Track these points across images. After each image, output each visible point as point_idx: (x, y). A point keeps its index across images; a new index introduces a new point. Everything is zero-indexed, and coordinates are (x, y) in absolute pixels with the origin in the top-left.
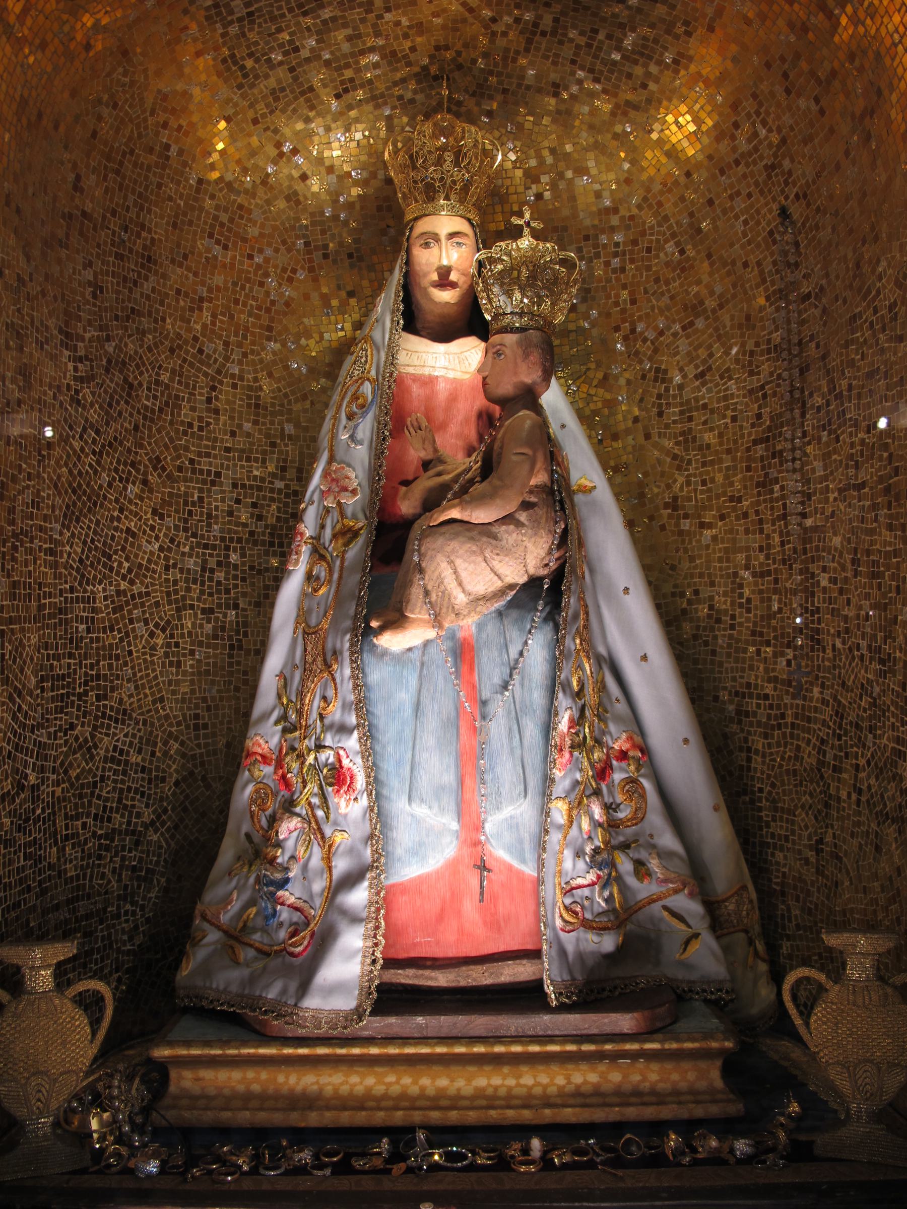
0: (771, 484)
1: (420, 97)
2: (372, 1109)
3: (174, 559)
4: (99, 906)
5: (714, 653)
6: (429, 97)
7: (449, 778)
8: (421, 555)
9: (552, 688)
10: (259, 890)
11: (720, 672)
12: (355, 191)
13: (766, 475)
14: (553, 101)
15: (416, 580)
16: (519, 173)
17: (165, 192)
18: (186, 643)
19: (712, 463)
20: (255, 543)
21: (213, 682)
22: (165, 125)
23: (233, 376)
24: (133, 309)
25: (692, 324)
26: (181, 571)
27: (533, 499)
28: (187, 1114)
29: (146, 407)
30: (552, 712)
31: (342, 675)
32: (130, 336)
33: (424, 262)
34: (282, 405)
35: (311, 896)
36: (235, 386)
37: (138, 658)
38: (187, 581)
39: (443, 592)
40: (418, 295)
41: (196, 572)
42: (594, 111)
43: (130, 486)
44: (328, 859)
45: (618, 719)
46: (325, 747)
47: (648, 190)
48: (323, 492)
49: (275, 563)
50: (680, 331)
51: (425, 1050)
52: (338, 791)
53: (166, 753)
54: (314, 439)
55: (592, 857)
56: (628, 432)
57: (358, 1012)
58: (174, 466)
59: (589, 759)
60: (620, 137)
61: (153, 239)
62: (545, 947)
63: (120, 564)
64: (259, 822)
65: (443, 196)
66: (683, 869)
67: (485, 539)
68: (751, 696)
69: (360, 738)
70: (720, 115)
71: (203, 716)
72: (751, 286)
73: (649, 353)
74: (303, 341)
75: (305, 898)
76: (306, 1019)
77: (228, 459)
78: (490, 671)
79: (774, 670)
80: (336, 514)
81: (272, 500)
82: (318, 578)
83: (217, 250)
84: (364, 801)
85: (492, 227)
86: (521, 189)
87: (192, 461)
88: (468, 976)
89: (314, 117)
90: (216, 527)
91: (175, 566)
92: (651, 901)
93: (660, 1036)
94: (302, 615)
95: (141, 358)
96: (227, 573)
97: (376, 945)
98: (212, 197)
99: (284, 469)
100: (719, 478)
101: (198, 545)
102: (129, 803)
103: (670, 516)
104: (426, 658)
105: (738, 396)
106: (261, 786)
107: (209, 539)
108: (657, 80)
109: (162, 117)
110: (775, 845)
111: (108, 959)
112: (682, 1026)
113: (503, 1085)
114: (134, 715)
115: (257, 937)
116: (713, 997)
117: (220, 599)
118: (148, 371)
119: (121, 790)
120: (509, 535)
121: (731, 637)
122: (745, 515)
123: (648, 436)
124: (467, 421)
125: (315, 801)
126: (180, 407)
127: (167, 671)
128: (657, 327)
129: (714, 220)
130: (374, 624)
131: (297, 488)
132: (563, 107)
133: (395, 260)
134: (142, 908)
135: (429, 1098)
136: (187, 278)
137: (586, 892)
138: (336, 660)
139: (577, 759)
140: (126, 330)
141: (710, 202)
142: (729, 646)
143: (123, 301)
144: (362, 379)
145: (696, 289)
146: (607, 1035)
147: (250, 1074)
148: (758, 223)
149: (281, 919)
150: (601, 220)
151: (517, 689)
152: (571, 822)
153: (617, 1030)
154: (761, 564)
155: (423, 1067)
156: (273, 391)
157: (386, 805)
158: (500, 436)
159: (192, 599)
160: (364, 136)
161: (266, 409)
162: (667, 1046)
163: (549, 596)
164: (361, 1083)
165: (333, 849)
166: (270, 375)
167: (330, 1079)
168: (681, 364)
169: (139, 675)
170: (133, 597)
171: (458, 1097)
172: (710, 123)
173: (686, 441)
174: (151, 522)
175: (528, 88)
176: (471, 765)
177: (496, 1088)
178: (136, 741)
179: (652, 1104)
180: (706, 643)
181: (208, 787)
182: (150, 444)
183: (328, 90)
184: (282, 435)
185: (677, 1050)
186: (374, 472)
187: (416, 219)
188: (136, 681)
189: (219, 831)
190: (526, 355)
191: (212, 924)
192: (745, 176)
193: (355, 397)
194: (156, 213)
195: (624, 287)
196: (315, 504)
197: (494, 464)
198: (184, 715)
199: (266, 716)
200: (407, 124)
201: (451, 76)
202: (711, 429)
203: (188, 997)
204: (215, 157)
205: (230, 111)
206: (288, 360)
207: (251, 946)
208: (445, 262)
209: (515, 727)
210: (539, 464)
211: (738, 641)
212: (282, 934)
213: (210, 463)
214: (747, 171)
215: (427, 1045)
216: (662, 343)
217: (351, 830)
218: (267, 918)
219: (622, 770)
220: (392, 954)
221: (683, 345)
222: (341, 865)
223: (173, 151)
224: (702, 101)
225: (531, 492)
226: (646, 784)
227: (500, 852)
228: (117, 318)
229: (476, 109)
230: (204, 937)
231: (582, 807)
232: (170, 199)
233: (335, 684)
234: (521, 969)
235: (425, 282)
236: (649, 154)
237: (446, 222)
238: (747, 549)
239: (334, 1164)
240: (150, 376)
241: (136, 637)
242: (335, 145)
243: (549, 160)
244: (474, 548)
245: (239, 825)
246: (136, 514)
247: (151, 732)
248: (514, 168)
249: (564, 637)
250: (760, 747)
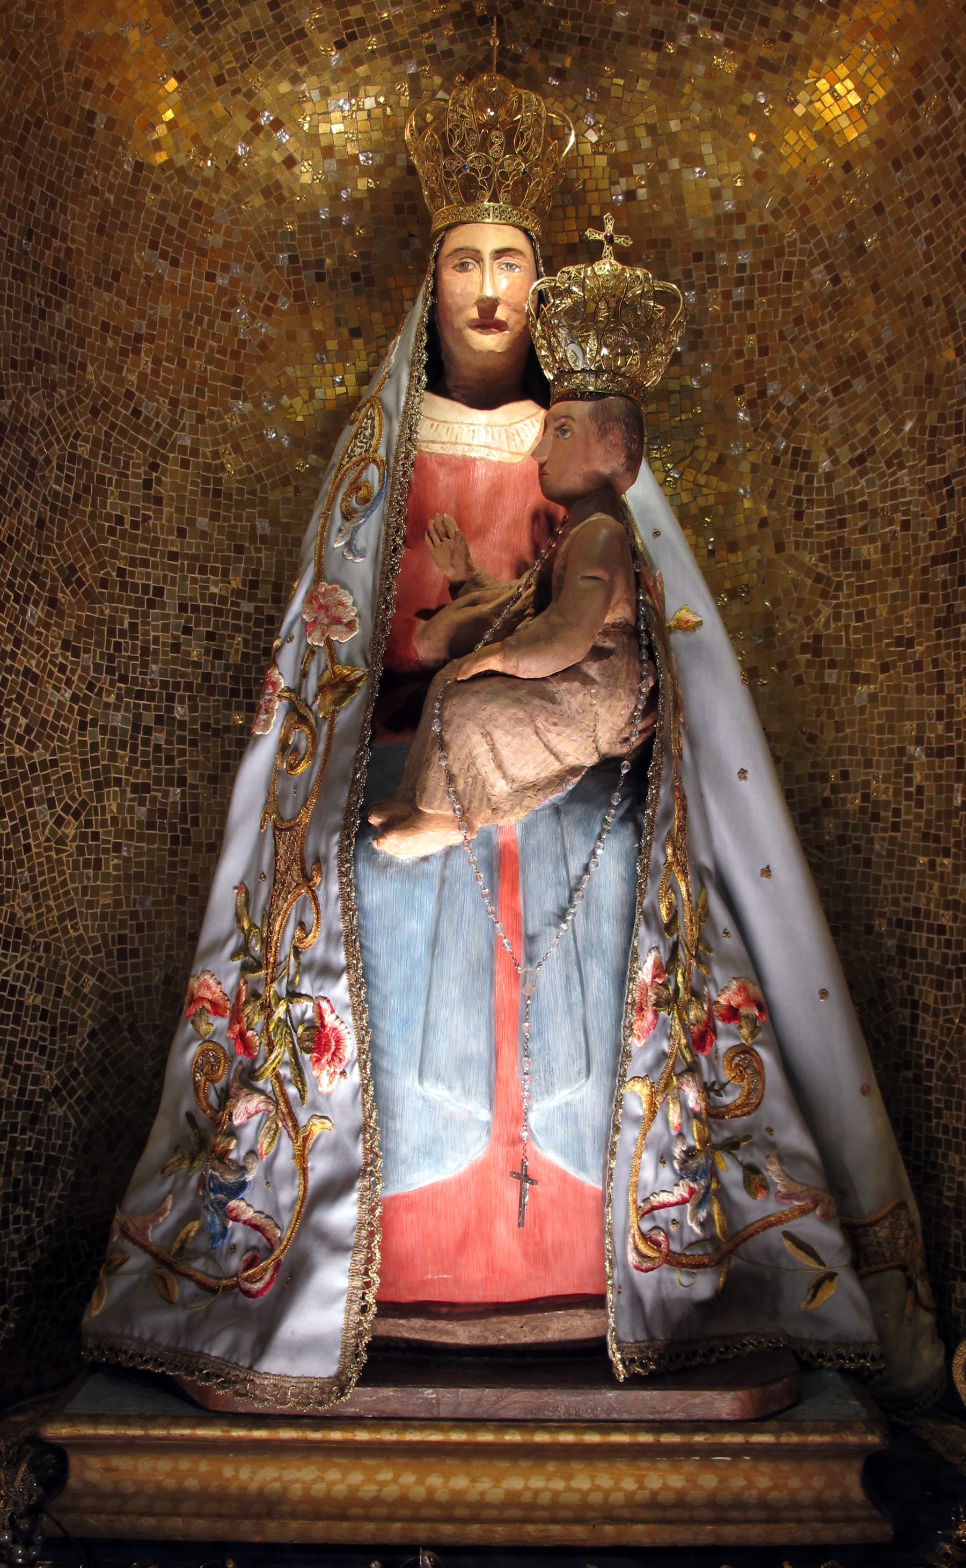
0: (957, 623)
1: (459, 48)
3: (93, 713)
5: (867, 863)
6: (472, 48)
7: (478, 1046)
8: (444, 724)
9: (633, 915)
10: (203, 1198)
11: (877, 892)
12: (364, 184)
13: (950, 608)
14: (652, 57)
15: (435, 759)
16: (602, 161)
17: (87, 181)
18: (108, 833)
19: (872, 588)
20: (211, 691)
21: (147, 891)
22: (88, 84)
23: (183, 449)
24: (38, 351)
25: (847, 385)
26: (104, 730)
27: (609, 644)
28: (92, 1520)
29: (56, 494)
30: (629, 955)
31: (327, 893)
32: (33, 391)
33: (458, 291)
34: (253, 493)
35: (277, 1210)
36: (185, 464)
37: (39, 855)
38: (111, 744)
39: (475, 778)
40: (449, 339)
41: (124, 731)
42: (712, 73)
43: (30, 608)
44: (301, 1157)
45: (727, 961)
46: (300, 995)
47: (789, 189)
48: (305, 624)
49: (239, 720)
50: (830, 395)
51: (435, 1437)
52: (318, 1060)
53: (77, 992)
54: (298, 542)
55: (683, 1162)
56: (751, 539)
57: (339, 1383)
58: (94, 578)
59: (682, 1020)
60: (751, 112)
61: (69, 250)
62: (610, 1296)
63: (15, 720)
64: (206, 1098)
65: (488, 195)
66: (816, 1181)
67: (537, 702)
68: (919, 927)
69: (351, 985)
70: (896, 81)
71: (132, 939)
72: (934, 333)
73: (785, 426)
74: (285, 400)
75: (268, 1212)
76: (264, 1390)
77: (173, 569)
78: (541, 892)
79: (954, 891)
80: (324, 657)
81: (237, 629)
82: (296, 749)
83: (163, 266)
84: (355, 1077)
85: (562, 239)
86: (604, 184)
87: (121, 572)
88: (500, 1331)
89: (306, 75)
90: (154, 667)
91: (94, 723)
92: (767, 1224)
93: (774, 1424)
94: (273, 801)
95: (49, 422)
96: (170, 734)
97: (367, 1285)
98: (156, 189)
99: (254, 585)
100: (882, 610)
101: (129, 692)
102: (23, 1063)
103: (810, 664)
104: (448, 872)
105: (912, 493)
106: (210, 1046)
107: (144, 684)
108: (805, 29)
109: (83, 72)
110: (948, 1143)
112: (805, 1411)
113: (546, 1489)
114: (32, 937)
115: (199, 1264)
116: (853, 1366)
117: (159, 770)
118: (58, 441)
119: (12, 1044)
120: (573, 697)
121: (893, 841)
122: (919, 666)
123: (780, 547)
124: (516, 524)
125: (286, 1072)
126: (105, 494)
127: (81, 874)
128: (797, 388)
129: (883, 237)
130: (375, 820)
131: (273, 613)
132: (667, 66)
133: (419, 285)
134: (40, 1212)
135: (439, 1505)
136: (118, 307)
137: (673, 1213)
138: (319, 870)
139: (665, 1021)
140: (28, 383)
141: (879, 209)
142: (890, 854)
143: (24, 340)
144: (366, 461)
145: (854, 335)
146: (698, 1421)
147: (184, 1464)
148: (948, 241)
149: (234, 1241)
150: (719, 232)
151: (580, 921)
152: (654, 1113)
153: (712, 1415)
154: (939, 738)
155: (432, 1460)
156: (240, 472)
157: (385, 1081)
158: (562, 550)
159: (118, 770)
160: (378, 103)
161: (229, 497)
162: (784, 1439)
163: (627, 786)
164: (342, 1481)
165: (310, 1143)
166: (237, 449)
167: (298, 1475)
168: (831, 443)
169: (40, 879)
170: (33, 767)
171: (482, 1504)
172: (881, 92)
173: (835, 555)
174: (61, 659)
175: (617, 36)
176: (511, 1028)
177: (537, 1493)
178: (34, 974)
179: (760, 1521)
180: (857, 849)
181: (137, 1040)
182: (60, 547)
183: (325, 36)
184: (253, 537)
185: (798, 1445)
186: (380, 596)
187: (449, 228)
188: (36, 888)
189: (150, 1104)
190: (603, 433)
192: (929, 172)
193: (356, 487)
194: (73, 212)
195: (751, 329)
196: (295, 641)
197: (554, 591)
198: (104, 937)
199: (218, 946)
200: (441, 87)
201: (504, 18)
202: (872, 540)
203: (98, 1348)
204: (161, 130)
205: (183, 66)
206: (263, 427)
207: (190, 1277)
208: (489, 292)
209: (575, 976)
210: (619, 594)
211: (903, 847)
212: (235, 1263)
213: (148, 574)
214: (934, 165)
215: (439, 1429)
216: (803, 412)
217: (336, 1117)
218: (213, 1238)
219: (730, 1034)
220: (391, 1296)
221: (834, 416)
222: (321, 1167)
223: (100, 123)
224: (870, 60)
225: (606, 633)
226: (765, 1055)
227: (549, 1153)
228: (14, 364)
229: (540, 67)
230: (124, 1261)
231: (669, 1091)
232: (95, 191)
233: (317, 906)
234: (577, 1322)
235: (459, 321)
236: (791, 137)
237: (491, 234)
238: (920, 715)
240: (63, 449)
241: (35, 826)
242: (336, 116)
243: (646, 143)
244: (521, 714)
245: (177, 1102)
246: (39, 648)
247: (56, 962)
248: (595, 153)
249: (649, 845)
250: (931, 1002)
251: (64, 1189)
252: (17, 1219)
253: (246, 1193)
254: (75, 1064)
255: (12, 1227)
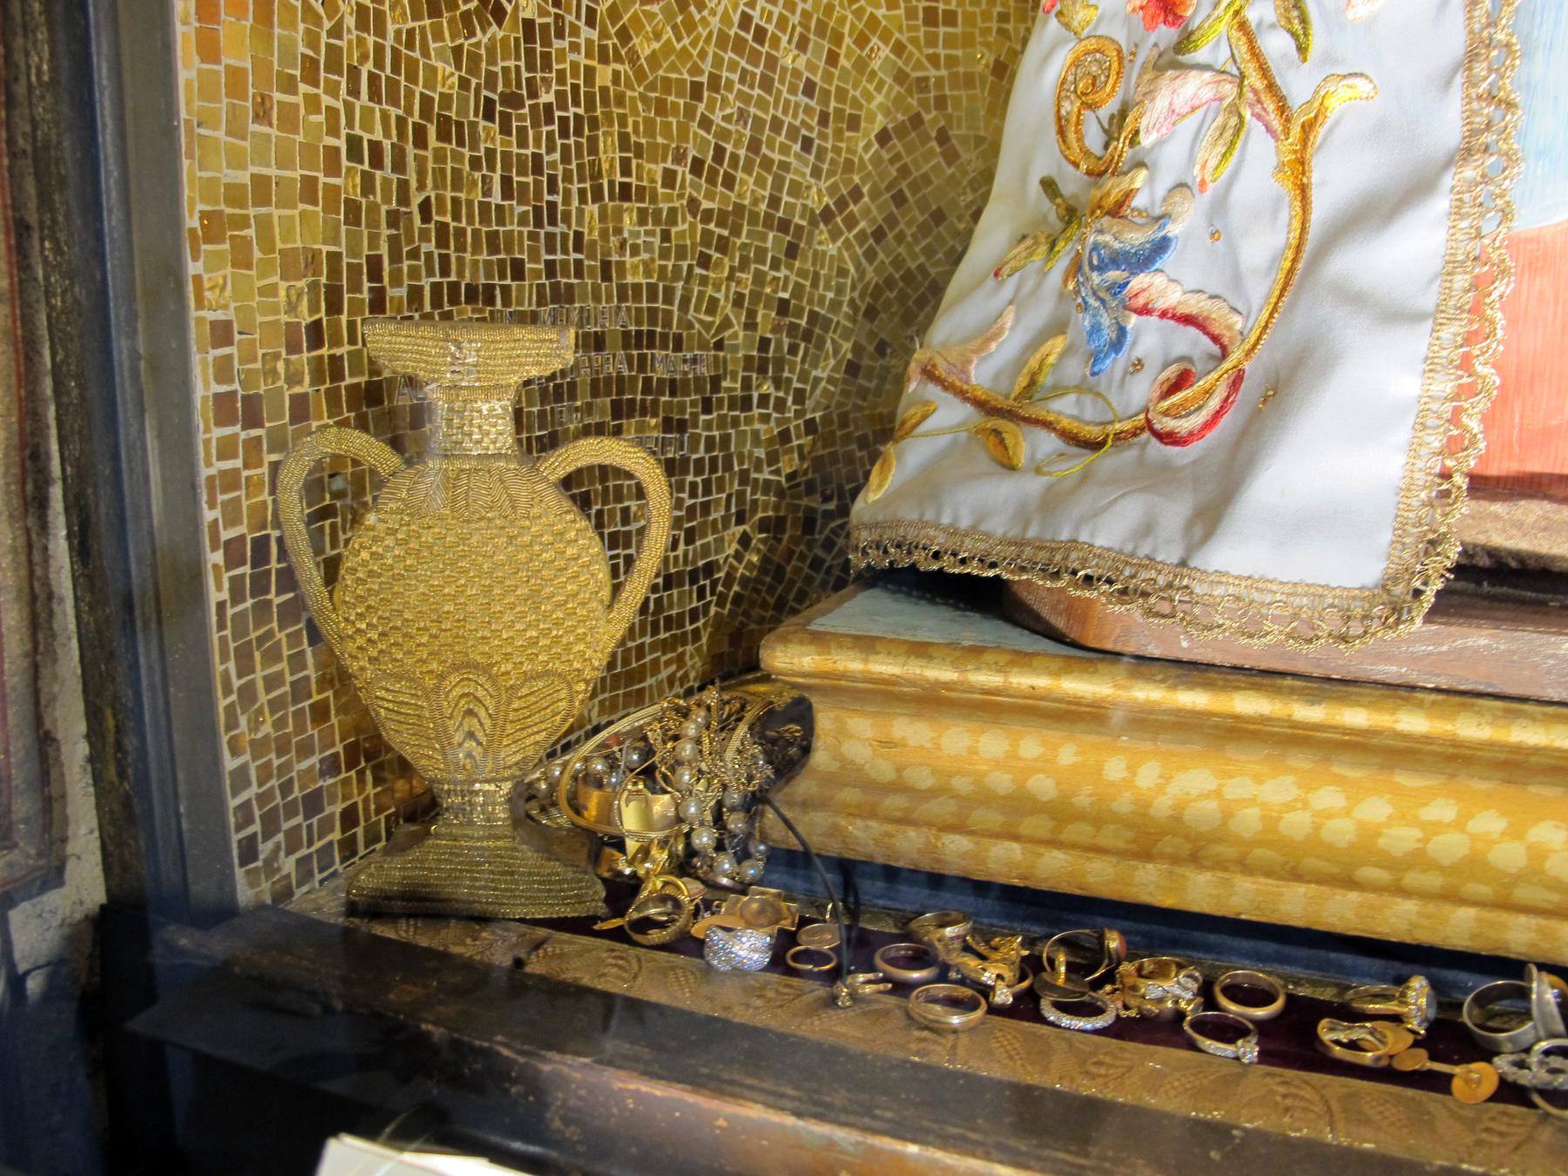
2: (1377, 888)
4: (704, 371)
44: (1298, 172)
53: (861, 65)
111: (721, 489)
134: (800, 397)
147: (1031, 746)
149: (1139, 352)
164: (1347, 812)
165: (1321, 131)
181: (951, 157)
191: (947, 387)
207: (1048, 425)
212: (1141, 390)
222: (1338, 178)
230: (925, 417)
239: (1262, 1026)
251: (834, 369)
252: (764, 400)
253: (1167, 261)
254: (856, 179)
255: (756, 411)
